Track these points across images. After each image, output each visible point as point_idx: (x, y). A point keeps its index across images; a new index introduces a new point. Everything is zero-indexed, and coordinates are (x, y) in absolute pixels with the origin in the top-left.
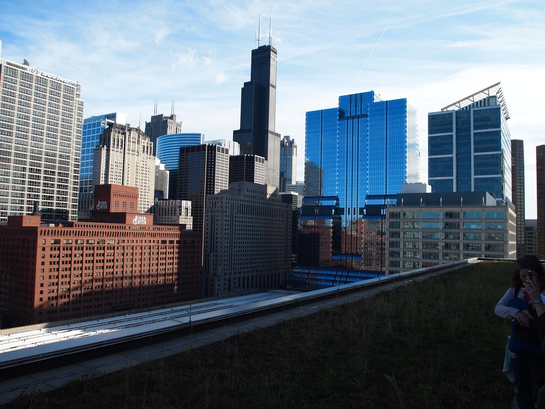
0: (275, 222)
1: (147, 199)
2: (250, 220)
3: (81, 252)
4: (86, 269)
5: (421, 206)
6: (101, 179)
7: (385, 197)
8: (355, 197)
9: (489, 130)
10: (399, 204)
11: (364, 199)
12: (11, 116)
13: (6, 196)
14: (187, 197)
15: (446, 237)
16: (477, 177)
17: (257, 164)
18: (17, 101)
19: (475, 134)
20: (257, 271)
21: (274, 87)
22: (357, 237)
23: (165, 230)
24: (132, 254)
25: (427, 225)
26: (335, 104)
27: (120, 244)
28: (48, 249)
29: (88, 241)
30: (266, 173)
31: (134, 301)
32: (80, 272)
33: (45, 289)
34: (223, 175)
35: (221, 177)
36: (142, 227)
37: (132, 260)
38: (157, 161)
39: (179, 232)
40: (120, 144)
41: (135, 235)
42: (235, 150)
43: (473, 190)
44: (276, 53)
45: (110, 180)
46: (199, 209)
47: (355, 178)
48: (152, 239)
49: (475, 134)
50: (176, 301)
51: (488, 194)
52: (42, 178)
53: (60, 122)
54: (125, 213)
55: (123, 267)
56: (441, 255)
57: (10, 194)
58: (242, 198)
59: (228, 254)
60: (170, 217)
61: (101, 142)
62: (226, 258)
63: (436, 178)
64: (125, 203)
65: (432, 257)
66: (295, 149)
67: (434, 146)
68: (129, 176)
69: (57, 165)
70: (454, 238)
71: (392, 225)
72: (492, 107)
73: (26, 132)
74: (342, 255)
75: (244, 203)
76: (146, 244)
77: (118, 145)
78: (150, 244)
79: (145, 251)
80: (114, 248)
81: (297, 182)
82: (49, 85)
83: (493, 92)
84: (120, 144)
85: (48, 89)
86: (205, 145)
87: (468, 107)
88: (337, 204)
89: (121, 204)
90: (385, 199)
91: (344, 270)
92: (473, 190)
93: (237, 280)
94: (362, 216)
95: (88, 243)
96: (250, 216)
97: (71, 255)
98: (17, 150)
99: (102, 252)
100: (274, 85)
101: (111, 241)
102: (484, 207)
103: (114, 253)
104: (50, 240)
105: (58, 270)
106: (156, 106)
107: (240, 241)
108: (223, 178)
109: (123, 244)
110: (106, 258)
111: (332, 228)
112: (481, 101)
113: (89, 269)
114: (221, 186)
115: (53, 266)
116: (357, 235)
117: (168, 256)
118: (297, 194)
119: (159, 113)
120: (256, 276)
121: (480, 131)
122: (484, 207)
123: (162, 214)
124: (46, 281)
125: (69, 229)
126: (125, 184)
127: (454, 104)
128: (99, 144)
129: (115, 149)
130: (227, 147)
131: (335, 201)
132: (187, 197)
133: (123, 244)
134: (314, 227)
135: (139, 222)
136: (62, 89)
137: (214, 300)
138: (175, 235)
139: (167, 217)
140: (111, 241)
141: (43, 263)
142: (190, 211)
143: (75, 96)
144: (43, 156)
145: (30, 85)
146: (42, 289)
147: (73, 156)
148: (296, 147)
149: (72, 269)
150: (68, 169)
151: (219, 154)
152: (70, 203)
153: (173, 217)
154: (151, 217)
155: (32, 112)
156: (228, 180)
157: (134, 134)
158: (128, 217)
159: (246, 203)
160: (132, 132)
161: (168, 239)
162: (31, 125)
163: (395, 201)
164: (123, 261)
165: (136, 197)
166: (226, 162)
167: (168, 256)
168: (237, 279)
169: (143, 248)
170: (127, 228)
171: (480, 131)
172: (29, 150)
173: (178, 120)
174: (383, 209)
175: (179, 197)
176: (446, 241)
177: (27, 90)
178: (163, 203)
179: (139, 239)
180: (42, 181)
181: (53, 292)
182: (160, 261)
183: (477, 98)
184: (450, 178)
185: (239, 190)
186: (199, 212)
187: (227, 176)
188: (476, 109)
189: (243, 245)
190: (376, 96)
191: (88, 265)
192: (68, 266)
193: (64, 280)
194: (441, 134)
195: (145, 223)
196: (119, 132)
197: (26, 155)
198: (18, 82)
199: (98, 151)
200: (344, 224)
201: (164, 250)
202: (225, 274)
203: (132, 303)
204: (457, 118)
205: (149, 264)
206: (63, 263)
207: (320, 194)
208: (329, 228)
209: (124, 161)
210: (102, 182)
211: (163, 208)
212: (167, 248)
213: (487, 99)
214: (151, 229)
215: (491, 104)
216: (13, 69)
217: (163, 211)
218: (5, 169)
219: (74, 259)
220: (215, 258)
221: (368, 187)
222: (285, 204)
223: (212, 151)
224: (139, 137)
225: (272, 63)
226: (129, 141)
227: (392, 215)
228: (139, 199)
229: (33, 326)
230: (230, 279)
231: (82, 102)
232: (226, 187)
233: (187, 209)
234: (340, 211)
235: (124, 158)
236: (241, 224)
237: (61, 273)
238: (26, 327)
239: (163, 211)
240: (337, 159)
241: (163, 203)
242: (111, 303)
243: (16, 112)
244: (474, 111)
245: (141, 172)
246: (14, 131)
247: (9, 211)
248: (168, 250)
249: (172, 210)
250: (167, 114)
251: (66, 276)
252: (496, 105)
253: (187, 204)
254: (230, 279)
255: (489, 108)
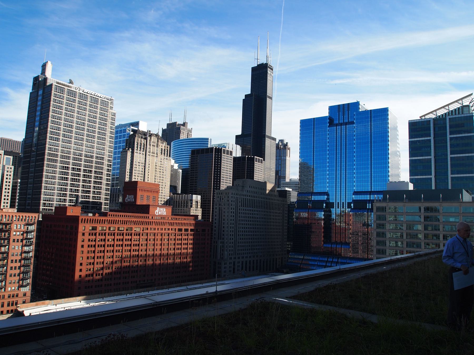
0: (273, 214)
1: (165, 193)
2: (252, 212)
3: (113, 237)
4: (116, 252)
5: (405, 201)
6: (127, 176)
7: (370, 193)
8: (343, 193)
9: (463, 135)
10: (384, 199)
11: (352, 194)
12: (59, 125)
13: (53, 190)
14: (196, 191)
15: (426, 228)
16: (453, 176)
17: (257, 165)
18: (63, 113)
19: (451, 139)
20: (243, 257)
21: (271, 98)
22: (345, 228)
23: (181, 220)
24: (154, 240)
25: (410, 218)
26: (326, 113)
27: (144, 231)
28: (87, 235)
29: (119, 228)
30: (264, 171)
31: (155, 279)
32: (112, 254)
33: (84, 268)
34: (227, 173)
35: (226, 175)
36: (163, 217)
37: (154, 245)
38: (173, 161)
39: (194, 222)
40: (142, 147)
41: (157, 223)
42: (237, 152)
43: (450, 188)
44: (272, 69)
45: (133, 177)
46: (207, 202)
47: (343, 176)
48: (170, 227)
49: (451, 139)
50: (189, 281)
51: (464, 192)
52: (82, 175)
53: (97, 130)
54: (149, 205)
55: (146, 251)
56: (423, 245)
57: (56, 189)
58: (245, 193)
59: (233, 241)
60: (183, 209)
61: (127, 145)
62: (231, 245)
63: (416, 177)
64: (148, 197)
65: (415, 246)
66: (288, 151)
67: (415, 149)
68: (150, 174)
69: (94, 165)
70: (432, 230)
71: (379, 218)
72: (466, 115)
73: (70, 138)
74: (332, 243)
75: (247, 197)
76: (165, 232)
77: (141, 148)
78: (168, 232)
79: (165, 237)
80: (139, 235)
81: (290, 180)
82: (89, 99)
83: (466, 102)
84: (142, 147)
85: (88, 103)
86: (213, 148)
87: (444, 115)
88: (328, 199)
89: (145, 198)
90: (370, 195)
91: (333, 256)
92: (450, 188)
93: (240, 264)
94: (350, 210)
95: (118, 230)
96: (252, 209)
97: (105, 240)
98: (50, 151)
99: (130, 237)
100: (271, 96)
101: (137, 229)
102: (461, 202)
103: (139, 239)
104: (89, 227)
105: (94, 252)
106: (171, 115)
107: (243, 230)
108: (227, 176)
109: (147, 231)
110: (133, 243)
111: (324, 219)
112: (455, 110)
113: (119, 252)
114: (226, 183)
115: (90, 249)
116: (345, 226)
117: (184, 242)
118: (291, 190)
119: (173, 121)
120: (257, 260)
121: (455, 136)
122: (461, 202)
123: (176, 206)
124: (85, 261)
125: (104, 218)
126: (146, 180)
127: (431, 112)
128: (125, 148)
129: (139, 152)
130: (230, 149)
131: (326, 197)
132: (196, 191)
133: (147, 231)
134: (308, 218)
135: (160, 213)
136: (99, 103)
137: (222, 280)
138: (190, 224)
139: (180, 208)
140: (137, 229)
141: (83, 246)
142: (199, 204)
143: (109, 108)
144: (83, 158)
145: (74, 100)
146: (81, 267)
147: (106, 158)
148: (289, 149)
149: (106, 251)
150: (102, 168)
151: (225, 156)
152: (103, 196)
153: (185, 209)
154: (170, 209)
155: (75, 122)
156: (232, 178)
157: (154, 139)
158: (151, 208)
159: (249, 198)
160: (152, 138)
161: (183, 228)
162: (74, 132)
163: (381, 196)
164: (147, 246)
165: (158, 192)
166: (230, 162)
167: (184, 242)
168: (241, 263)
169: (163, 234)
170: (150, 217)
171: (455, 136)
172: (72, 153)
173: (189, 126)
174: (369, 203)
175: (190, 192)
176: (426, 232)
177: (72, 104)
178: (177, 196)
179: (160, 227)
180: (81, 178)
181: (90, 270)
182: (177, 246)
183: (452, 108)
184: (429, 177)
185: (243, 187)
186: (207, 205)
187: (231, 174)
188: (452, 117)
189: (245, 233)
190: (361, 106)
191: (118, 248)
192: (102, 249)
193: (99, 260)
194: (421, 139)
195: (165, 214)
196: (142, 138)
197: (69, 157)
198: (65, 98)
199: (124, 153)
200: (334, 216)
201: (180, 237)
202: (231, 258)
203: (153, 281)
204: (434, 124)
205: (168, 249)
206: (98, 246)
207: (313, 190)
208: (320, 219)
209: (145, 161)
210: (127, 179)
211: (177, 201)
212: (183, 235)
213: (461, 108)
214: (170, 218)
215: (465, 113)
216: (61, 87)
217: (176, 203)
218: (53, 168)
219: (107, 243)
220: (221, 245)
221: (355, 184)
222: (281, 199)
223: (218, 153)
224: (158, 141)
225: (269, 78)
226: (150, 145)
227: (379, 209)
228: (160, 194)
229: (74, 298)
230: (234, 263)
231: (115, 114)
232: (230, 183)
233: (197, 202)
234: (330, 205)
235: (145, 158)
236: (244, 215)
237: (97, 255)
238: (69, 299)
239: (176, 203)
240: (328, 160)
241: (177, 196)
242: (136, 281)
243: (63, 122)
244: (449, 119)
245: (159, 170)
246: (61, 138)
247: (55, 203)
248: (184, 237)
249: (184, 203)
250: (180, 122)
251: (100, 257)
252: (469, 113)
253: (197, 198)
254: (234, 263)
255: (463, 115)
